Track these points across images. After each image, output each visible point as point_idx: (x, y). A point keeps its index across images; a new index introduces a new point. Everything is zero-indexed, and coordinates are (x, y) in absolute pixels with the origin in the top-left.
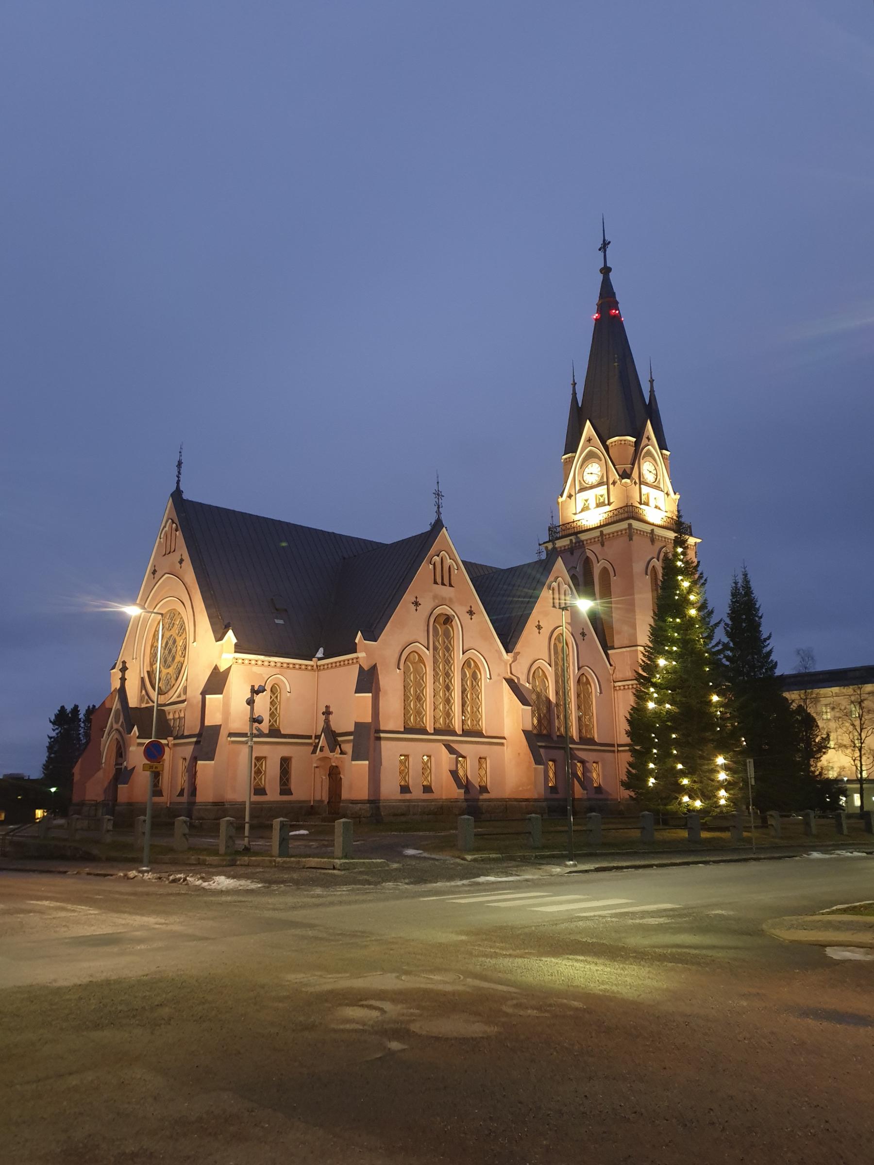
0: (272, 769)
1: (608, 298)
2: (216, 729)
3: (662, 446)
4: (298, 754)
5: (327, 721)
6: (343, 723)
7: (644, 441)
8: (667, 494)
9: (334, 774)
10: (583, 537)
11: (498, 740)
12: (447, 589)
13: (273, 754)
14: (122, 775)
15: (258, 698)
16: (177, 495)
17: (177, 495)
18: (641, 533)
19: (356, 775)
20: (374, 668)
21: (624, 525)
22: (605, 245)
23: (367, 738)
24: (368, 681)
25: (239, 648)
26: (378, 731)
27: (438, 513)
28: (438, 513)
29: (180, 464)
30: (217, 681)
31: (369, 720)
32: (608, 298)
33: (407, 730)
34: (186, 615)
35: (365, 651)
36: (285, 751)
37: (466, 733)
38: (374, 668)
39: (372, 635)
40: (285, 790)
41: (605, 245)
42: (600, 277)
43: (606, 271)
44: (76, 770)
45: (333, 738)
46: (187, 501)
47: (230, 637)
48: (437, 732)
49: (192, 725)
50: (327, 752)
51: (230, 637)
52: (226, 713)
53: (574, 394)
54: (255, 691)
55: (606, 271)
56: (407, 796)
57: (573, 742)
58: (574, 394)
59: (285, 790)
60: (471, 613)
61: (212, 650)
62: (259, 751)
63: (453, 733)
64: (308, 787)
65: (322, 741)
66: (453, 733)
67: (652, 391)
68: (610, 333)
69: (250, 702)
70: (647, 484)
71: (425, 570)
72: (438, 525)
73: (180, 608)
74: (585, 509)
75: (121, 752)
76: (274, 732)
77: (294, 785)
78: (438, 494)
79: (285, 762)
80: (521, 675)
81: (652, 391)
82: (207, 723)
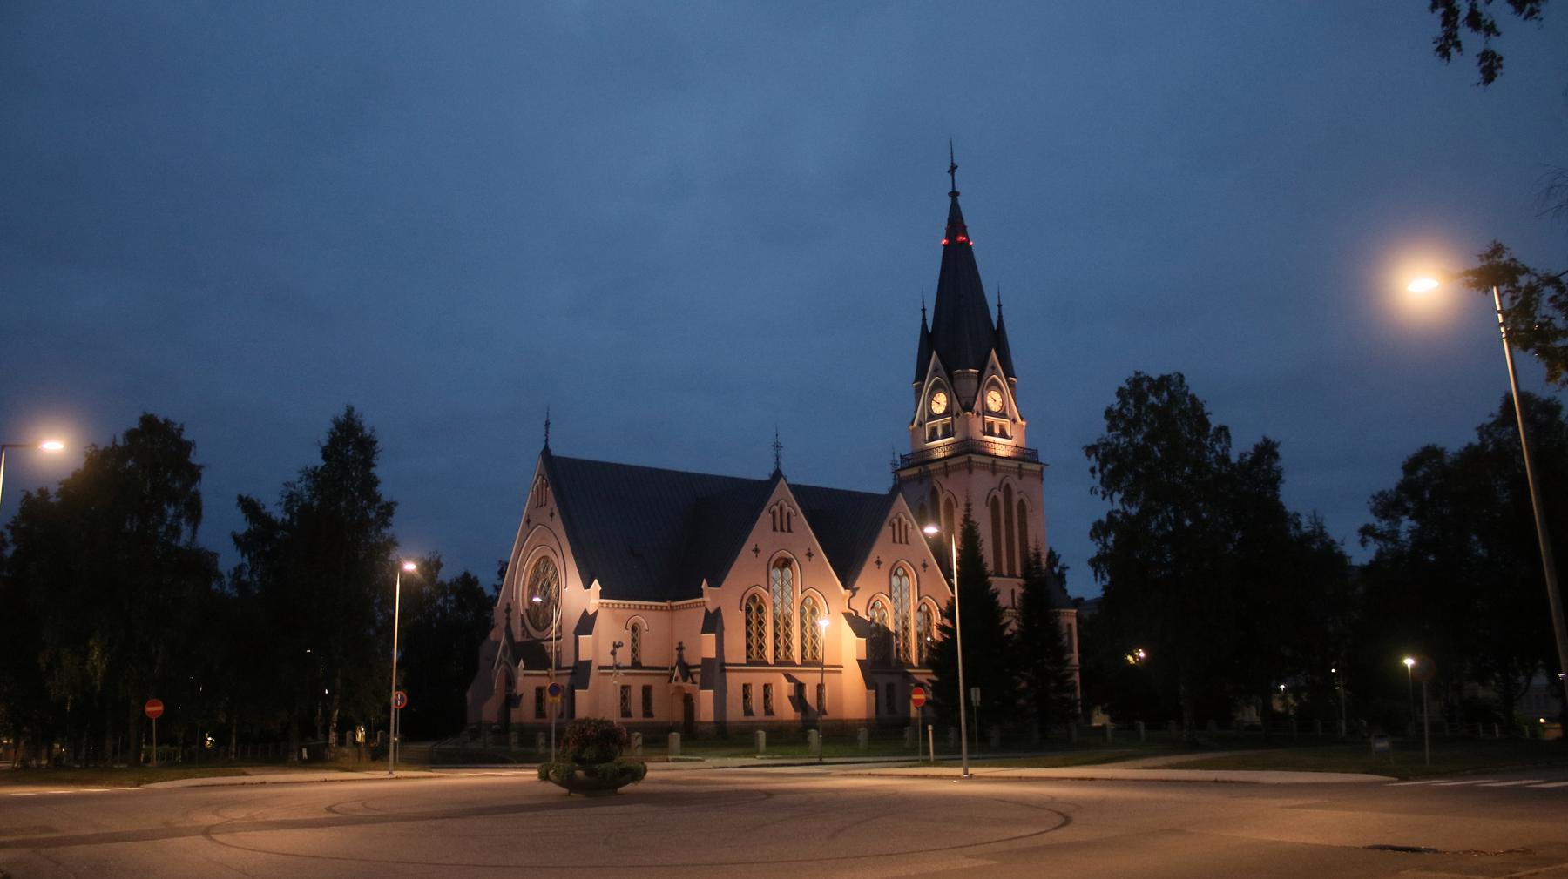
0: (636, 697)
1: (956, 224)
2: (588, 663)
3: (1009, 372)
4: (657, 683)
5: (680, 656)
6: (693, 659)
7: (988, 369)
8: (1014, 421)
9: (689, 702)
10: (931, 467)
11: (837, 669)
12: (786, 534)
13: (637, 683)
14: (512, 701)
15: (618, 651)
16: (546, 452)
17: (546, 452)
18: (982, 466)
19: (706, 701)
20: (718, 610)
21: (964, 459)
22: (953, 169)
23: (713, 672)
24: (713, 622)
25: (603, 595)
26: (723, 664)
27: (778, 463)
28: (778, 463)
29: (547, 424)
30: (586, 623)
31: (713, 655)
32: (956, 224)
33: (750, 662)
34: (559, 563)
35: (710, 597)
36: (646, 681)
37: (804, 663)
38: (718, 610)
39: (716, 582)
40: (647, 711)
41: (953, 169)
42: (948, 201)
43: (954, 194)
44: (469, 695)
45: (686, 670)
46: (559, 458)
47: (596, 586)
48: (777, 663)
49: (568, 661)
50: (680, 682)
51: (596, 586)
52: (596, 651)
53: (924, 320)
54: (616, 646)
55: (954, 194)
56: (751, 718)
57: (912, 666)
58: (924, 320)
59: (647, 711)
60: (810, 555)
61: (579, 596)
62: (628, 681)
63: (794, 664)
64: (665, 710)
65: (677, 672)
66: (794, 664)
67: (1000, 316)
68: (958, 262)
69: (613, 653)
70: (991, 413)
71: (765, 519)
72: (777, 475)
73: (552, 556)
74: (933, 437)
75: (510, 681)
76: (636, 664)
77: (655, 711)
78: (777, 446)
79: (647, 690)
80: (860, 606)
81: (1000, 316)
82: (581, 658)
